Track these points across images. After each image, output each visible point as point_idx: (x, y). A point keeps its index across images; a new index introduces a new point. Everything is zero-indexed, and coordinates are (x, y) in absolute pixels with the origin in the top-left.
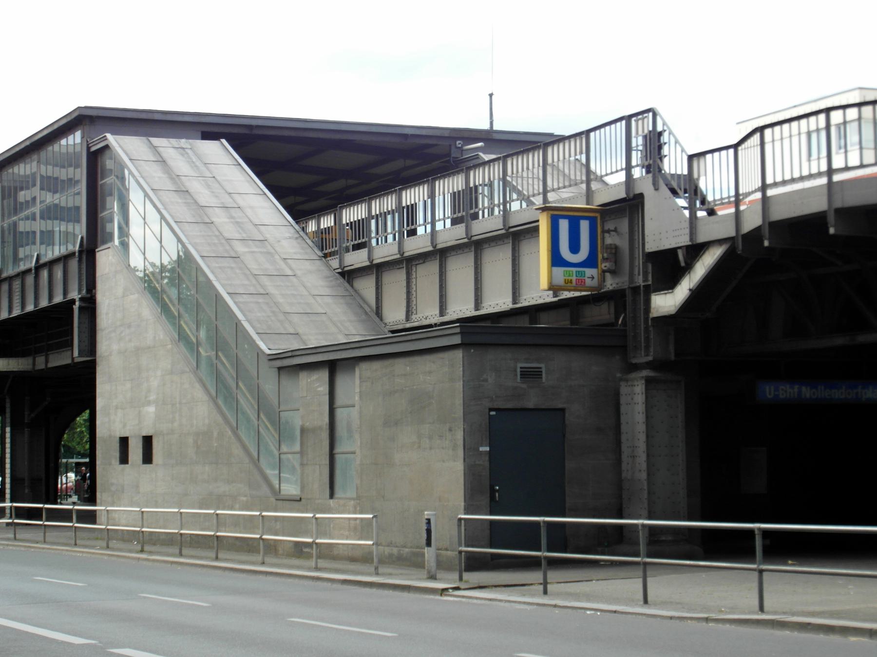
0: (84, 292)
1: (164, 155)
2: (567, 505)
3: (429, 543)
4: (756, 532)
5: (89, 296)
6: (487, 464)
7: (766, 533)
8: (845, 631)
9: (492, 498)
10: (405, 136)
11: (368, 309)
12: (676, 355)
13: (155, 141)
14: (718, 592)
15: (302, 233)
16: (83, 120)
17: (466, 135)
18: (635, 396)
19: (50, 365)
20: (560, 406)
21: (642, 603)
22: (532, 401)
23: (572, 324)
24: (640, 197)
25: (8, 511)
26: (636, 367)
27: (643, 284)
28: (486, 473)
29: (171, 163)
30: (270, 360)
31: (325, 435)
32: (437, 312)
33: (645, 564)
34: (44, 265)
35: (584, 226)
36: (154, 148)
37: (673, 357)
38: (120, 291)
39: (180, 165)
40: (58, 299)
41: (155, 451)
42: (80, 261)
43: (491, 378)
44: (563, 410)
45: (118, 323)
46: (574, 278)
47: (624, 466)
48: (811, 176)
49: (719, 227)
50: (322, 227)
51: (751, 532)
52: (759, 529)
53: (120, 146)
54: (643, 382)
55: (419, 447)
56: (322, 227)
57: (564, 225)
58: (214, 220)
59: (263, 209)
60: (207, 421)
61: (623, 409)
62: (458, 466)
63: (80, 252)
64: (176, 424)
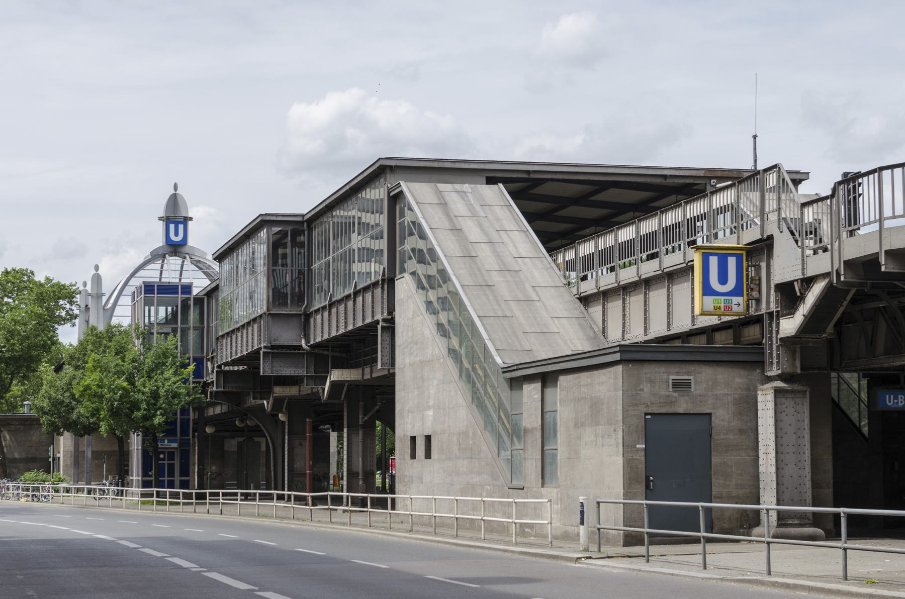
0: (385, 314)
1: (448, 199)
2: (713, 493)
3: (582, 523)
8: (796, 587)
11: (596, 329)
12: (802, 369)
13: (441, 186)
14: (813, 562)
15: (553, 264)
16: (381, 171)
17: (719, 174)
18: (766, 400)
20: (707, 411)
23: (735, 343)
24: (771, 238)
26: (770, 379)
28: (642, 466)
29: (452, 206)
31: (538, 435)
32: (643, 332)
33: (331, 509)
34: (359, 291)
35: (732, 262)
36: (439, 193)
37: (799, 371)
38: (410, 315)
39: (458, 206)
40: (369, 320)
42: (383, 288)
43: (647, 388)
44: (710, 414)
45: (410, 340)
46: (722, 305)
47: (761, 462)
48: (870, 223)
53: (410, 192)
57: (714, 261)
58: (479, 254)
60: (465, 423)
62: (620, 460)
63: (383, 280)
64: (446, 425)
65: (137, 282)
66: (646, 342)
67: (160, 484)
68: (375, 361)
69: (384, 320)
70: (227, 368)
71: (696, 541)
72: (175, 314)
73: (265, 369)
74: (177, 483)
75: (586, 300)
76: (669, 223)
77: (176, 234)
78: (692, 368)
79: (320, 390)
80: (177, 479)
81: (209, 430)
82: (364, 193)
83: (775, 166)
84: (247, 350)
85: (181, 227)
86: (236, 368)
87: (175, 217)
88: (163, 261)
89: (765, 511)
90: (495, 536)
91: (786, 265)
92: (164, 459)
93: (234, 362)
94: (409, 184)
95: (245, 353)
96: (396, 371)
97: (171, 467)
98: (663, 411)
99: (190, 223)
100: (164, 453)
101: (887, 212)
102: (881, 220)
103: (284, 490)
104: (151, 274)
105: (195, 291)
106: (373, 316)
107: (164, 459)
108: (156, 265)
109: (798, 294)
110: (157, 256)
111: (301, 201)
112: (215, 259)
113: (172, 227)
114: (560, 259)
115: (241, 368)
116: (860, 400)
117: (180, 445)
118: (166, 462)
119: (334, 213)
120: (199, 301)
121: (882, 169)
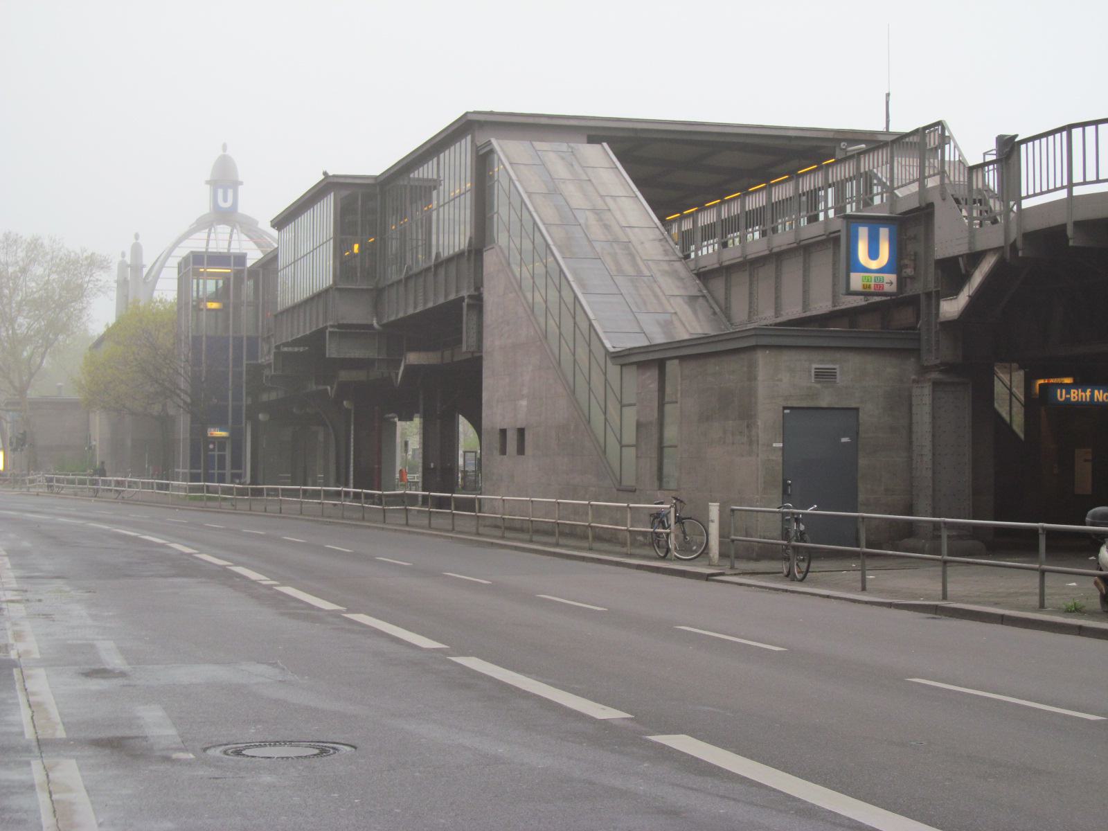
0: (472, 290)
4: (1040, 531)
5: (476, 293)
6: (780, 459)
7: (1049, 533)
9: (785, 492)
10: (789, 138)
13: (536, 144)
16: (467, 126)
17: (850, 136)
19: (456, 359)
20: (854, 405)
21: (860, 589)
22: (826, 400)
24: (931, 206)
25: (420, 499)
27: (934, 290)
28: (779, 468)
30: (614, 357)
32: (773, 314)
40: (452, 297)
41: (526, 443)
42: (469, 259)
44: (857, 409)
46: (873, 284)
48: (1056, 189)
49: (992, 238)
50: (683, 229)
51: (1034, 531)
52: (1044, 529)
54: (930, 384)
55: (724, 442)
56: (683, 229)
59: (631, 210)
61: (914, 410)
63: (470, 252)
65: (182, 252)
66: (776, 325)
67: (209, 478)
68: (460, 341)
69: (470, 297)
70: (286, 349)
71: (856, 555)
72: (226, 286)
73: (333, 350)
74: (228, 477)
75: (704, 276)
76: (806, 188)
77: (225, 200)
78: (838, 355)
79: (393, 375)
80: (228, 471)
81: (261, 417)
82: (416, 172)
83: (939, 123)
84: (311, 328)
85: (230, 193)
86: (296, 349)
87: (224, 178)
88: (210, 230)
89: (861, 520)
90: (606, 546)
91: (949, 237)
92: (213, 450)
93: (296, 342)
94: (500, 141)
95: (308, 333)
96: (484, 355)
97: (222, 459)
98: (804, 404)
99: (240, 188)
100: (214, 443)
101: (1077, 178)
102: (1071, 185)
103: (347, 485)
104: (197, 244)
105: (249, 263)
106: (457, 292)
107: (213, 450)
108: (203, 235)
109: (963, 271)
110: (205, 224)
111: (373, 161)
112: (273, 226)
113: (220, 192)
114: (675, 230)
115: (301, 349)
116: (1011, 394)
117: (232, 434)
118: (216, 453)
119: (412, 176)
120: (253, 272)
121: (1069, 128)
